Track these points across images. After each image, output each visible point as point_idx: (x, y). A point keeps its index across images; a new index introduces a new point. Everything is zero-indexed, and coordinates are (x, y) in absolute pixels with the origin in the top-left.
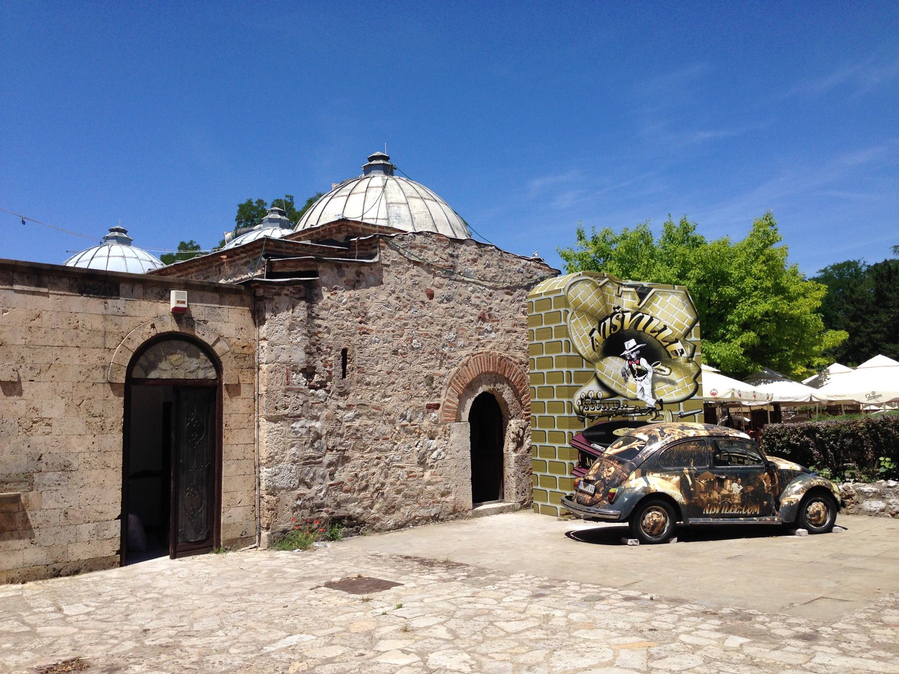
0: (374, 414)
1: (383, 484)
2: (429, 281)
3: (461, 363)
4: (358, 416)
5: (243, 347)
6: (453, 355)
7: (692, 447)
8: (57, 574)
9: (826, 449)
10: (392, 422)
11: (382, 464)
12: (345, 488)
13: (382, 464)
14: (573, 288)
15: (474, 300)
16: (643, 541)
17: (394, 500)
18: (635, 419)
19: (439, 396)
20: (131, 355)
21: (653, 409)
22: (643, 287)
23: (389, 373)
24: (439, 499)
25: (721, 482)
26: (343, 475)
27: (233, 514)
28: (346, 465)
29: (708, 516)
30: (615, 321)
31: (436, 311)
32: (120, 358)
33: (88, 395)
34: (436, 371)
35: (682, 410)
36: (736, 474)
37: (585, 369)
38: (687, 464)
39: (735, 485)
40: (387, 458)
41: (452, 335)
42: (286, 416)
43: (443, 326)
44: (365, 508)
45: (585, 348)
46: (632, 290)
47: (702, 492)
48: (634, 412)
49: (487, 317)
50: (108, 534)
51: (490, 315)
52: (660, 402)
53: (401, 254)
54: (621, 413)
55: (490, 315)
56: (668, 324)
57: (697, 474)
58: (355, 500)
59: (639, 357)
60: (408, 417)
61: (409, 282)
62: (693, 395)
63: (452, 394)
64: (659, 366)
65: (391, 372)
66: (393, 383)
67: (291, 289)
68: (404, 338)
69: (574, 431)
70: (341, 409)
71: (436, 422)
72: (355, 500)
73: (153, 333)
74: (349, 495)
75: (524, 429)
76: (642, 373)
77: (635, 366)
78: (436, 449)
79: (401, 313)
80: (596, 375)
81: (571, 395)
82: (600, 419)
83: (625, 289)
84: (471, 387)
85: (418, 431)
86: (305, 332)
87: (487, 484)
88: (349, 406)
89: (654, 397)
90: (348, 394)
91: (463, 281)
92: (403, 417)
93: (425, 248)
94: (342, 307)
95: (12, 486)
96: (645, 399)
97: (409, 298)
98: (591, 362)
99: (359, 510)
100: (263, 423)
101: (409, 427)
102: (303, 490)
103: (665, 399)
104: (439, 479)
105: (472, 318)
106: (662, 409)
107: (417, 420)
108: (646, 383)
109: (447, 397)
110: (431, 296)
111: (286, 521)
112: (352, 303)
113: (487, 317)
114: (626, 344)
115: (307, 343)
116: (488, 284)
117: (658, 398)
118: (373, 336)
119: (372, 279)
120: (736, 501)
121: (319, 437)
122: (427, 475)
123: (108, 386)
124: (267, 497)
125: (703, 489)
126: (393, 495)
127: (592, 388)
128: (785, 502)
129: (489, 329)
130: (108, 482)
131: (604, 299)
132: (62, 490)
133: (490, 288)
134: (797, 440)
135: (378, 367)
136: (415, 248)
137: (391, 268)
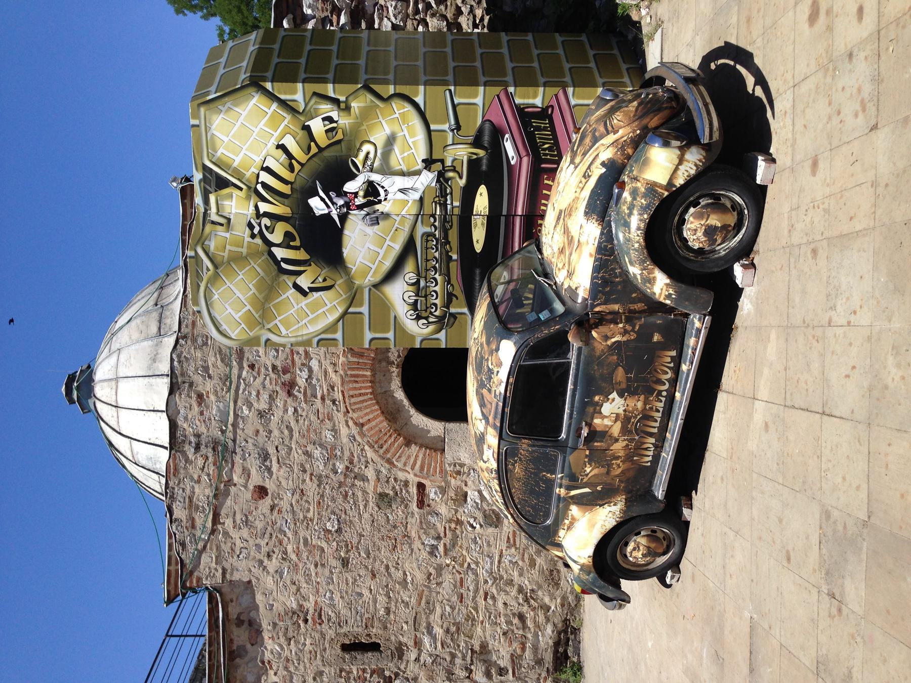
1: (521, 590)
2: (240, 498)
3: (358, 438)
6: (347, 454)
7: (518, 470)
10: (440, 569)
11: (494, 591)
12: (519, 651)
13: (494, 591)
14: (224, 327)
15: (263, 406)
17: (541, 571)
18: (456, 204)
21: (441, 175)
22: (205, 180)
23: (374, 576)
25: (594, 435)
28: (490, 647)
29: (656, 458)
30: (276, 237)
31: (284, 483)
34: (370, 488)
35: (446, 127)
36: (584, 405)
37: (364, 309)
38: (550, 484)
39: (607, 409)
40: (486, 582)
41: (317, 453)
43: (305, 471)
44: (548, 620)
46: (212, 198)
47: (608, 473)
48: (444, 206)
49: (287, 377)
51: (285, 371)
52: (428, 163)
53: (205, 547)
54: (445, 232)
55: (285, 371)
56: (273, 142)
58: (536, 635)
59: (341, 194)
60: (433, 542)
61: (245, 533)
63: (403, 459)
64: (359, 161)
65: (372, 571)
66: (387, 567)
68: (324, 545)
70: (419, 655)
71: (443, 491)
72: (536, 635)
74: (528, 645)
76: (372, 190)
77: (359, 201)
78: (480, 492)
79: (290, 548)
80: (376, 286)
82: (454, 280)
83: (213, 209)
84: (392, 414)
85: (453, 526)
88: (416, 643)
89: (418, 173)
90: (400, 643)
91: (235, 425)
93: (191, 501)
94: (287, 653)
96: (421, 188)
97: (267, 535)
98: (353, 299)
99: (549, 629)
101: (447, 540)
103: (422, 153)
105: (291, 410)
106: (442, 161)
107: (438, 525)
108: (392, 185)
109: (408, 468)
110: (262, 491)
112: (281, 634)
113: (287, 377)
114: (318, 213)
116: (235, 371)
117: (420, 165)
118: (324, 601)
119: (245, 600)
120: (640, 405)
125: (604, 470)
126: (535, 572)
127: (398, 293)
129: (305, 374)
131: (238, 259)
133: (241, 368)
135: (366, 592)
136: (193, 520)
137: (227, 566)
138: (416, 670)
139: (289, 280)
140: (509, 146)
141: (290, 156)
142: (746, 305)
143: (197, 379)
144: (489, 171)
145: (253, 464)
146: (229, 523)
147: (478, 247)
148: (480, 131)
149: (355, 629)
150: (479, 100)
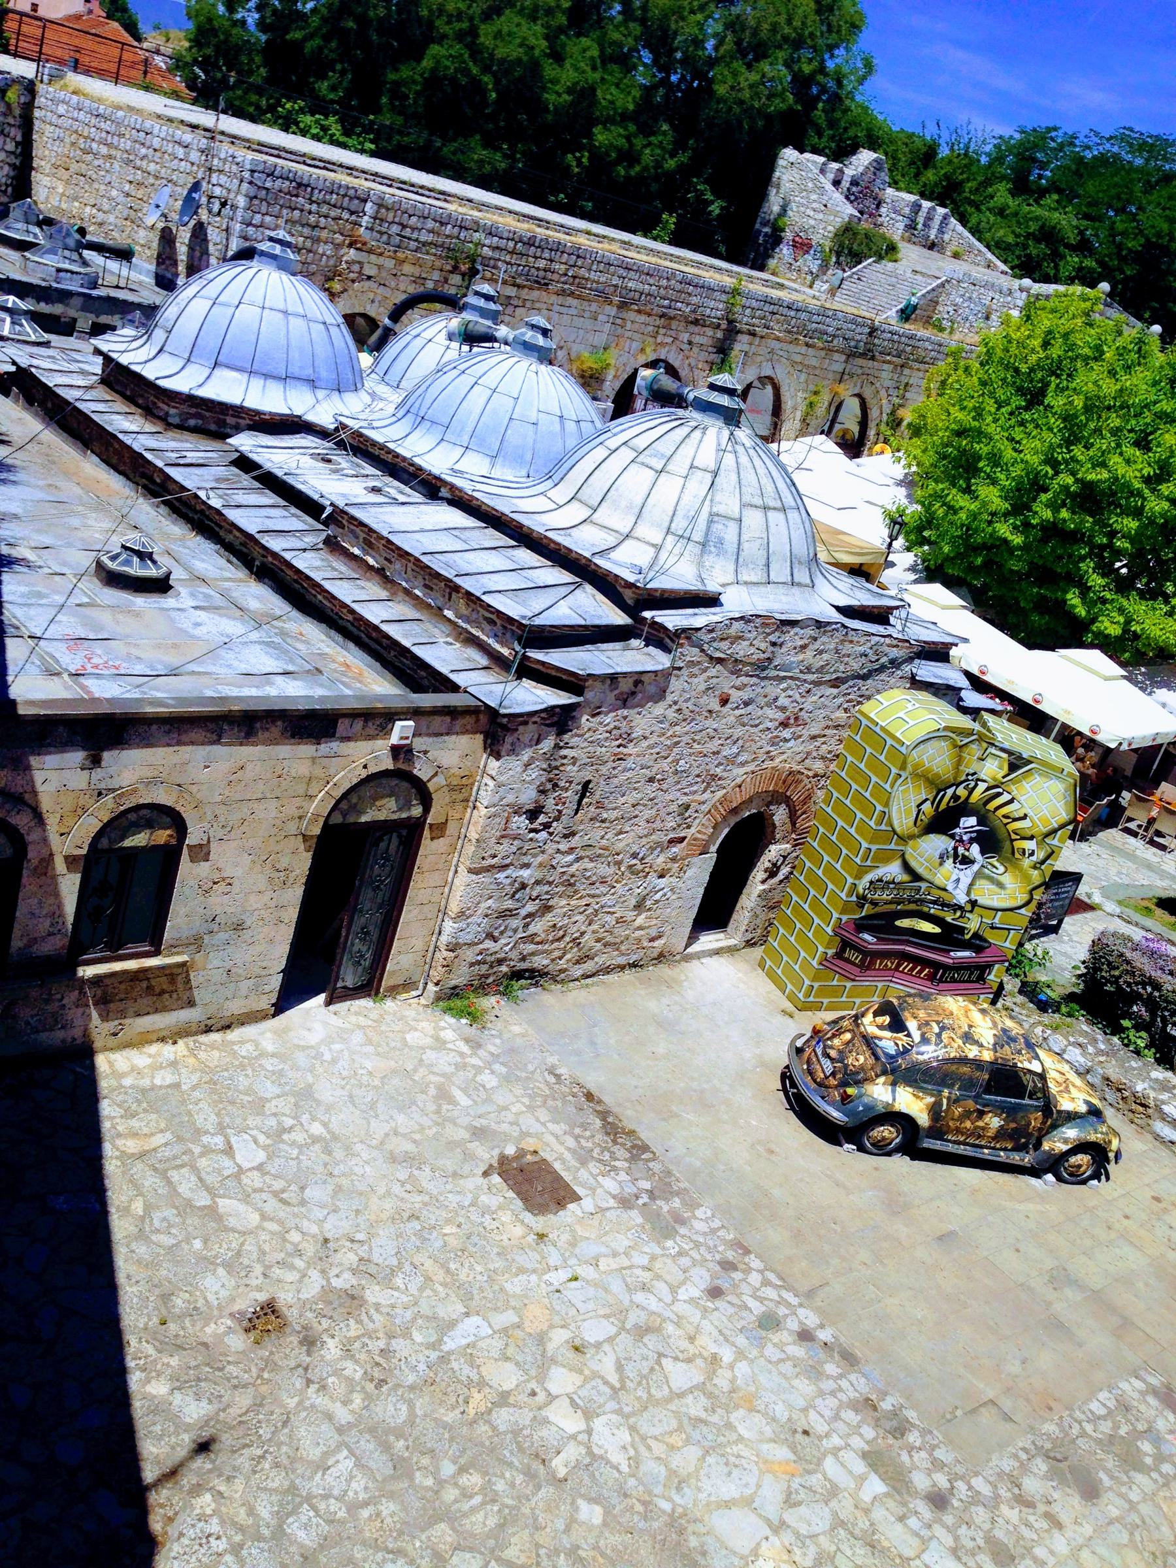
0: (599, 856)
1: (583, 934)
2: (726, 682)
4: (578, 859)
6: (725, 775)
7: (965, 1069)
8: (208, 1030)
9: (1156, 1016)
12: (538, 939)
16: (861, 1149)
19: (689, 827)
21: (961, 908)
24: (645, 944)
25: (981, 1114)
26: (538, 927)
27: (402, 958)
30: (962, 792)
32: (319, 805)
33: (278, 848)
35: (996, 920)
37: (892, 846)
39: (996, 1120)
42: (493, 866)
45: (903, 820)
46: (1005, 756)
48: (934, 902)
50: (267, 988)
51: (796, 719)
52: (974, 903)
56: (1030, 813)
57: (957, 1101)
59: (971, 841)
61: (702, 687)
62: (1020, 908)
64: (994, 861)
69: (845, 918)
73: (364, 774)
75: (785, 857)
76: (967, 861)
77: (961, 850)
79: (677, 728)
81: (861, 872)
83: (993, 751)
84: (735, 811)
86: (545, 766)
87: (714, 912)
89: (968, 894)
92: (634, 856)
95: (180, 949)
98: (903, 839)
99: (545, 962)
100: (462, 869)
102: (488, 944)
103: (982, 901)
104: (654, 922)
105: (770, 725)
111: (460, 977)
114: (963, 820)
115: (543, 779)
117: (973, 897)
118: (629, 763)
121: (523, 886)
122: (640, 920)
123: (300, 838)
124: (446, 954)
127: (893, 870)
128: (1046, 1146)
130: (278, 938)
132: (230, 949)
134: (1129, 984)
135: (623, 800)
138: (550, 851)
139: (931, 797)
140: (967, 954)
141: (1015, 820)
142: (1033, 1181)
143: (817, 645)
144: (951, 936)
145: (745, 695)
146: (713, 672)
147: (898, 923)
148: (986, 941)
149: (599, 790)
150: (1007, 944)
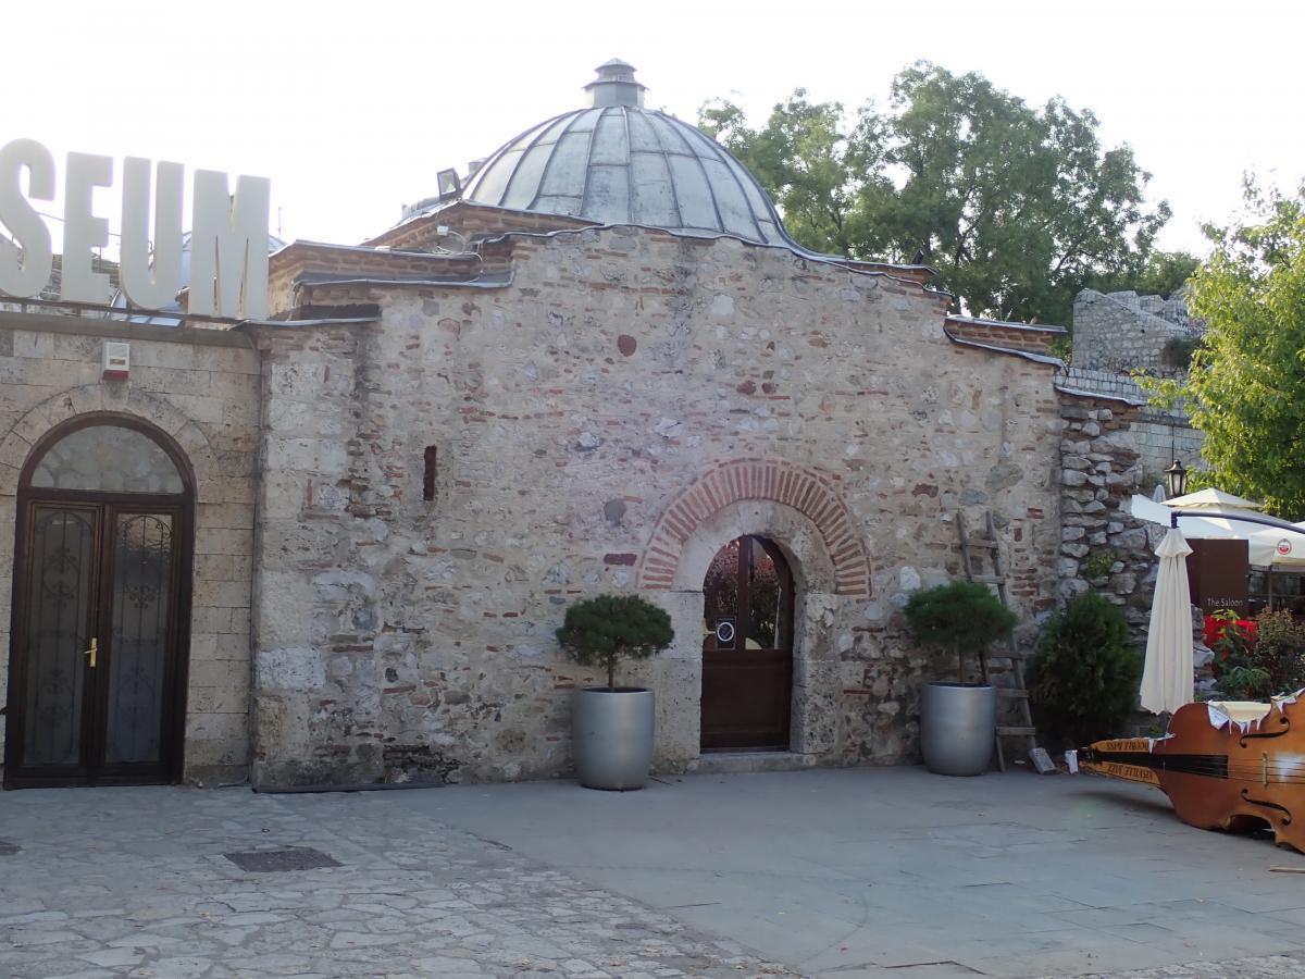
5: (236, 440)
20: (28, 449)
67: (323, 337)
73: (68, 414)
